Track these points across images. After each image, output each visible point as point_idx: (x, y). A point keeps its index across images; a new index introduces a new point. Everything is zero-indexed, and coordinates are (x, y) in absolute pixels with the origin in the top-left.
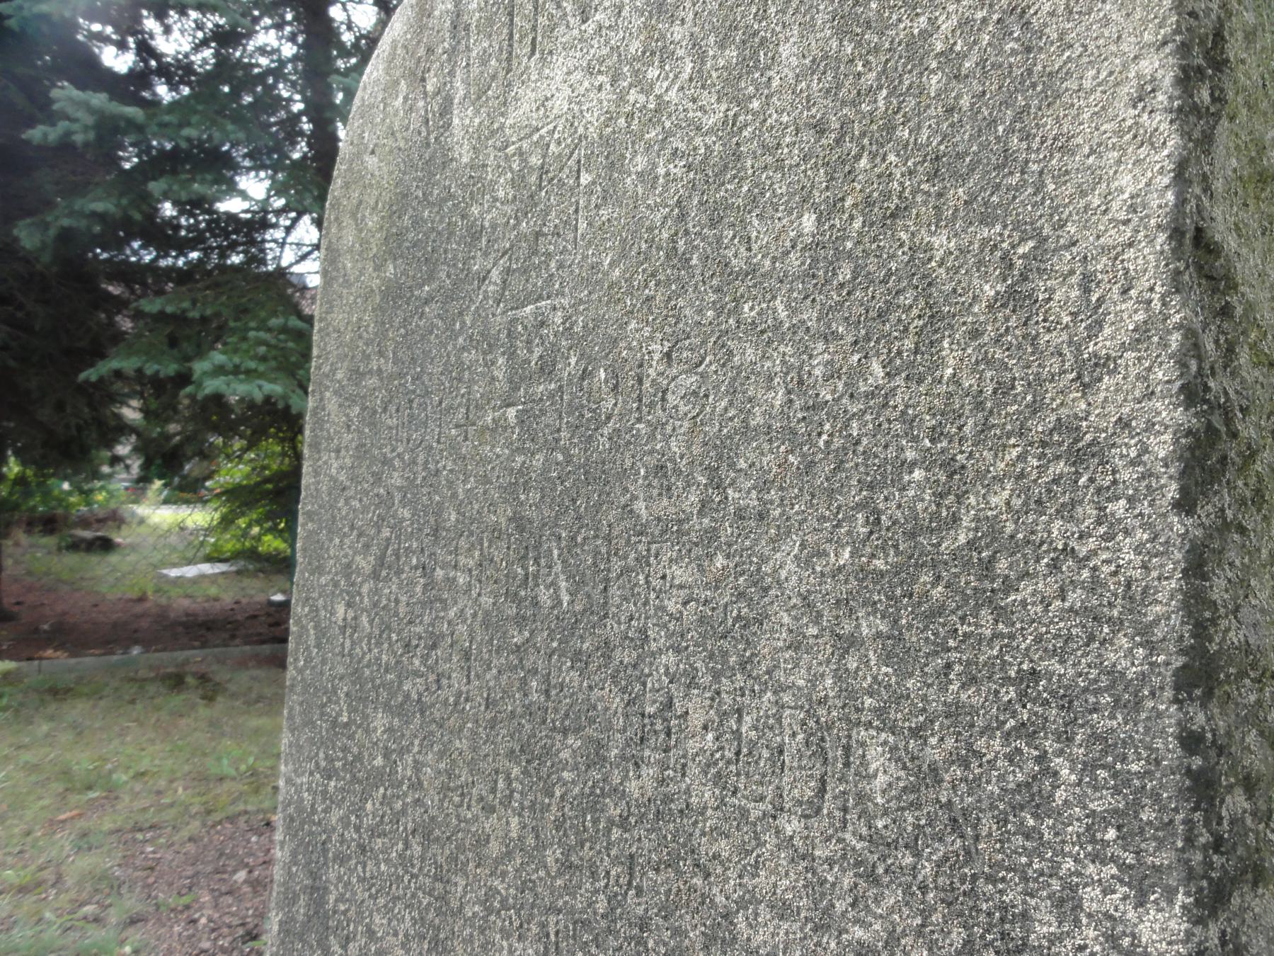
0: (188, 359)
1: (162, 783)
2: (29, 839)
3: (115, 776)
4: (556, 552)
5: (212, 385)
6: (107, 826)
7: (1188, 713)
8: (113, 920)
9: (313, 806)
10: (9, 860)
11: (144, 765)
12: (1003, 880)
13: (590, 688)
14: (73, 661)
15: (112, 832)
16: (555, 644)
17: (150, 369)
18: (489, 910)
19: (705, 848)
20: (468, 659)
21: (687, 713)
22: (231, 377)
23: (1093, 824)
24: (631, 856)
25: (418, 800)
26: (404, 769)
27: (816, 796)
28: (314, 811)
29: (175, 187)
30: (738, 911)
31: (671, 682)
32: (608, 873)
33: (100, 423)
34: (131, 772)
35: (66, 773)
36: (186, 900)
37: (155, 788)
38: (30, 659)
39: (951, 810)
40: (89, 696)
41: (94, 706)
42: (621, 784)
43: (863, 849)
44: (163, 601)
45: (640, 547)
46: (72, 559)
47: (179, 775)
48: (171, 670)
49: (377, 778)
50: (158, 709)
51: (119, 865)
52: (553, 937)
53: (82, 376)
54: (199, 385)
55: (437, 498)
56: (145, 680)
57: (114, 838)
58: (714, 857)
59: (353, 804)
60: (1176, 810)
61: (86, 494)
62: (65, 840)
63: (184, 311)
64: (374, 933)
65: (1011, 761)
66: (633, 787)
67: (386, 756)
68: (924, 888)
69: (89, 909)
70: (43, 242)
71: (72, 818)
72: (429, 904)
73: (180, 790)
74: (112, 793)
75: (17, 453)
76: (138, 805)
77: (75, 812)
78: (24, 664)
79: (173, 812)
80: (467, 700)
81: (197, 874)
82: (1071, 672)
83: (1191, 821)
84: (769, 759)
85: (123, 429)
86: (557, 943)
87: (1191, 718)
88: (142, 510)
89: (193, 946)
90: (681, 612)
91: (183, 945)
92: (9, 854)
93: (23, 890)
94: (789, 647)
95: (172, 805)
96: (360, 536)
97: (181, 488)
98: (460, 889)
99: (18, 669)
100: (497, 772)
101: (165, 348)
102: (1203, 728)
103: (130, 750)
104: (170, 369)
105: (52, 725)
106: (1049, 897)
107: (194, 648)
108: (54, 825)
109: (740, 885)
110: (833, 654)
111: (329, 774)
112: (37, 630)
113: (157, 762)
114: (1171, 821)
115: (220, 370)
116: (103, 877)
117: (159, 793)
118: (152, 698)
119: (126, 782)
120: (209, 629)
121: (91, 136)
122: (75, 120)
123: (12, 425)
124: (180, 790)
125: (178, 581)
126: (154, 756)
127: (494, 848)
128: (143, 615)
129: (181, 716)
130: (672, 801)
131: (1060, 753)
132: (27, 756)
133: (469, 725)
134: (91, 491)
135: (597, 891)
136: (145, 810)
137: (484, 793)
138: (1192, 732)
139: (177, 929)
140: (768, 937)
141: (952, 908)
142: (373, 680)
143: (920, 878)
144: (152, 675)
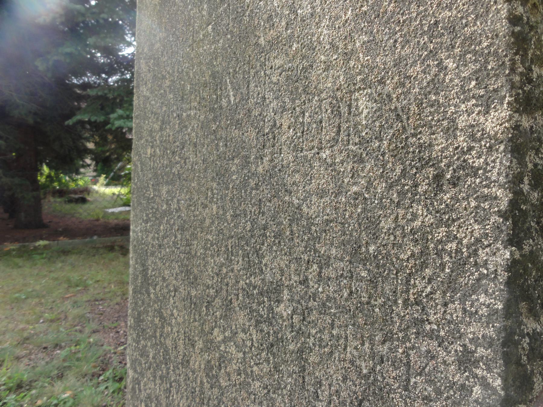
1: (106, 284)
2: (55, 304)
3: (87, 282)
4: (228, 81)
5: (118, 123)
6: (85, 299)
7: (514, 6)
8: (87, 331)
9: (142, 237)
10: (47, 311)
11: (99, 277)
12: (420, 133)
13: (243, 134)
14: (70, 241)
15: (86, 302)
16: (229, 122)
17: (93, 119)
18: (206, 249)
19: (289, 180)
20: (196, 147)
21: (282, 125)
22: (126, 120)
23: (464, 84)
24: (260, 200)
25: (179, 216)
26: (174, 205)
27: (336, 135)
28: (143, 239)
30: (303, 203)
31: (275, 114)
32: (251, 212)
34: (94, 281)
35: (69, 281)
36: (115, 325)
37: (103, 286)
38: (54, 240)
39: (396, 111)
40: (77, 254)
41: (79, 257)
42: (255, 170)
43: (356, 149)
45: (262, 59)
46: (72, 205)
47: (112, 281)
48: (109, 244)
49: (165, 213)
50: (104, 258)
51: (89, 313)
52: (230, 250)
53: (66, 123)
54: (113, 124)
55: (183, 82)
56: (99, 248)
57: (87, 304)
58: (293, 184)
59: (156, 229)
60: (506, 56)
62: (68, 304)
63: (106, 94)
64: (165, 278)
65: (425, 73)
66: (260, 169)
67: (167, 204)
68: (383, 155)
69: (78, 328)
71: (71, 296)
72: (184, 257)
73: (113, 286)
74: (86, 288)
75: (47, 165)
76: (96, 292)
78: (51, 242)
79: (110, 295)
80: (196, 165)
81: (119, 316)
82: (455, 12)
83: (514, 59)
84: (316, 128)
85: (87, 151)
86: (232, 251)
87: (516, 9)
88: (96, 187)
89: (118, 341)
90: (279, 80)
91: (114, 340)
92: (47, 309)
93: (52, 321)
94: (324, 71)
95: (110, 292)
96: (155, 115)
97: (113, 179)
98: (195, 246)
99: (49, 244)
100: (208, 190)
102: (522, 15)
103: (93, 272)
104: (101, 119)
105: (63, 264)
106: (442, 131)
107: (118, 236)
108: (64, 299)
109: (304, 191)
110: (343, 63)
111: (146, 222)
113: (103, 277)
114: (503, 63)
115: (121, 117)
116: (83, 316)
117: (105, 288)
118: (101, 254)
119: (91, 284)
120: (124, 230)
123: (42, 148)
124: (113, 286)
125: (113, 213)
126: (102, 275)
127: (208, 222)
129: (113, 261)
130: (276, 167)
131: (448, 57)
132: (52, 275)
133: (197, 175)
134: (77, 180)
135: (247, 222)
136: (99, 294)
137: (203, 201)
138: (516, 15)
139: (111, 335)
140: (316, 209)
141: (396, 158)
142: (161, 174)
143: (382, 150)
144: (101, 246)
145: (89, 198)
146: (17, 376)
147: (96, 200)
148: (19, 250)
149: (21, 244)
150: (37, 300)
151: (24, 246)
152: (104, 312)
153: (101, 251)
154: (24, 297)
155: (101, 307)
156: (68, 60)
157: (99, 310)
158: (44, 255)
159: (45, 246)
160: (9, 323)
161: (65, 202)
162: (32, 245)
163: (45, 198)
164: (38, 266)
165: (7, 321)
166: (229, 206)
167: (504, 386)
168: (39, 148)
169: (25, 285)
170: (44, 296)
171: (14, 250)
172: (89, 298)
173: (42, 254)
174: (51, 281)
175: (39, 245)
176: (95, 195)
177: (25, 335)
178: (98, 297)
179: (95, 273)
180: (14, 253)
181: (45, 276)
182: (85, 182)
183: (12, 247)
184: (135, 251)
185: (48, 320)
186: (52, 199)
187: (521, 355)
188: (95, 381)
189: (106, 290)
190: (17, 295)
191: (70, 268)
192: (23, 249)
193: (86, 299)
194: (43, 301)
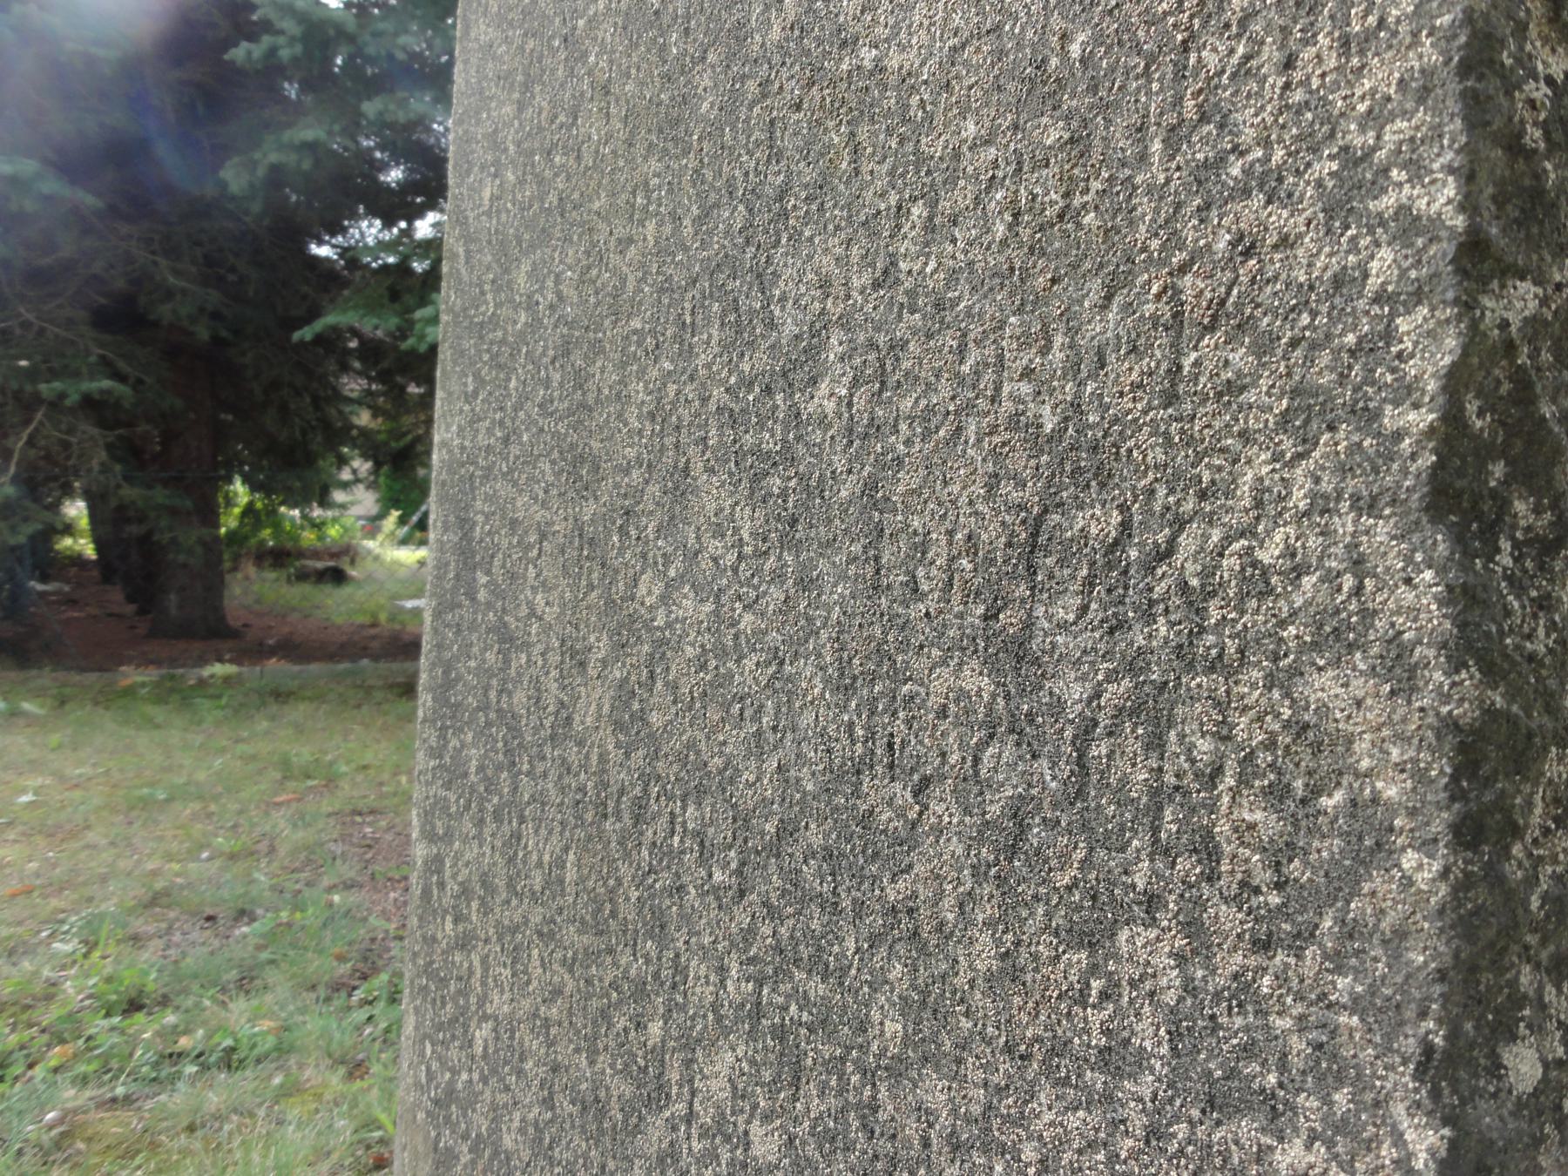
0: (411, 310)
11: (369, 757)
14: (296, 668)
15: (329, 815)
29: (392, 107)
33: (326, 425)
34: (353, 765)
35: (285, 764)
40: (310, 699)
41: (317, 709)
44: (397, 627)
46: (306, 588)
56: (371, 687)
57: (332, 821)
61: (318, 526)
62: (280, 821)
70: (252, 185)
71: (289, 801)
75: (246, 480)
77: (291, 796)
93: (233, 857)
95: (395, 794)
99: (239, 674)
101: (386, 301)
112: (261, 644)
121: (298, 49)
122: (281, 32)
123: (230, 417)
128: (374, 637)
132: (241, 748)
139: (392, 895)
145: (353, 573)
146: (129, 978)
147: (370, 578)
148: (157, 685)
149: (164, 671)
150: (197, 806)
151: (172, 677)
152: (377, 840)
153: (378, 695)
154: (162, 797)
155: (368, 830)
156: (307, 165)
157: (364, 837)
158: (224, 701)
159: (227, 680)
160: (118, 856)
161: (289, 581)
162: (192, 675)
163: (235, 569)
164: (204, 726)
165: (113, 851)
166: (690, 199)
167: (1467, 196)
168: (223, 416)
169: (167, 770)
170: (216, 798)
171: (143, 685)
172: (337, 807)
173: (219, 697)
174: (239, 763)
175: (212, 676)
176: (369, 565)
177: (159, 885)
178: (361, 805)
180: (144, 691)
181: (223, 750)
182: (346, 530)
183: (139, 679)
184: (442, 500)
185: (222, 854)
186: (251, 570)
187: (1522, 122)
188: (339, 1001)
189: (384, 789)
190: (145, 791)
191: (290, 731)
192: (169, 684)
193: (330, 809)
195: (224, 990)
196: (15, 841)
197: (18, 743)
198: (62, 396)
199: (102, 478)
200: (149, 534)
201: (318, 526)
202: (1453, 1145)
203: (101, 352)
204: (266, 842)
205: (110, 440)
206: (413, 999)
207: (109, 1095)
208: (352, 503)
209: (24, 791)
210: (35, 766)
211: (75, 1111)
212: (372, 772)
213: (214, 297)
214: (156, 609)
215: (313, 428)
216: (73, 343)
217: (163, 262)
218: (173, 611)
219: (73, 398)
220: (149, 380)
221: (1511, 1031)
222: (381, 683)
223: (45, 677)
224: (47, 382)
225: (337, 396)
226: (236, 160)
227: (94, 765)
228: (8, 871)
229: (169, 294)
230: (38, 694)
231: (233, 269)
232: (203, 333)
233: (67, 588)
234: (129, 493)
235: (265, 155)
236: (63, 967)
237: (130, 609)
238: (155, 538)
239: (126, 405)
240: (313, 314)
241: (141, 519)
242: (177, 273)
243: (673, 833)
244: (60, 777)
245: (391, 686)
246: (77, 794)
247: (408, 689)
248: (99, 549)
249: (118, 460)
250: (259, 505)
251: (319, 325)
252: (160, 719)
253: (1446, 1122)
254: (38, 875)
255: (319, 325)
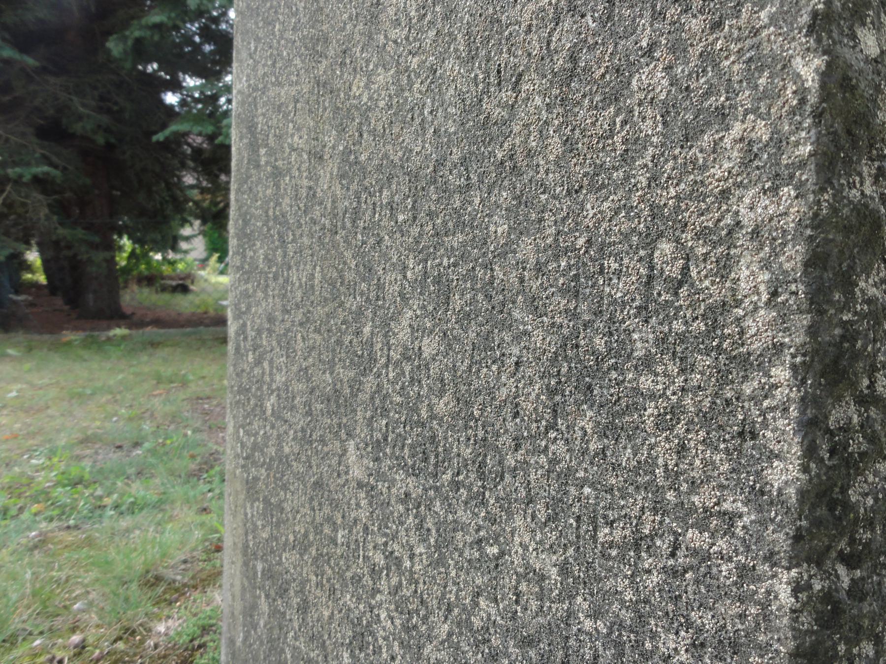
11: (205, 372)
33: (174, 199)
40: (171, 346)
46: (166, 296)
53: (155, 138)
62: (156, 402)
99: (130, 335)
123: (119, 193)
132: (132, 370)
147: (203, 290)
149: (87, 333)
150: (110, 397)
151: (92, 336)
152: (212, 411)
158: (122, 347)
159: (124, 338)
162: (103, 336)
163: (126, 287)
171: (76, 340)
172: (188, 395)
173: (119, 345)
175: (115, 336)
177: (89, 432)
178: (201, 395)
179: (198, 370)
180: (77, 343)
186: (135, 287)
190: (80, 390)
193: (184, 397)
194: (118, 397)
195: (128, 478)
196: (7, 415)
197: (6, 368)
198: (21, 176)
199: (46, 223)
200: (75, 255)
201: (172, 263)
202: (829, 65)
203: (42, 152)
204: (149, 413)
205: (49, 201)
206: (232, 411)
207: (66, 525)
208: (191, 250)
209: (11, 391)
210: (15, 380)
211: (47, 533)
212: (207, 379)
213: (105, 119)
214: (83, 301)
215: (167, 202)
216: (25, 146)
217: (75, 98)
218: (91, 304)
219: (27, 178)
220: (70, 168)
221: (862, 20)
222: (211, 337)
223: (20, 337)
224: (13, 168)
225: (180, 185)
226: (115, 36)
227: (50, 379)
228: (3, 428)
229: (80, 118)
230: (15, 346)
231: (116, 103)
232: (100, 140)
233: (30, 298)
234: (62, 231)
235: (132, 33)
236: (37, 471)
237: (67, 308)
238: (79, 258)
239: (58, 181)
240: (164, 126)
241: (69, 247)
242: (84, 105)
243: (375, 214)
244: (32, 385)
245: (217, 339)
246: (41, 392)
247: (224, 341)
248: (48, 278)
249: (54, 213)
250: (138, 251)
251: (167, 132)
252: (86, 357)
253: (825, 53)
254: (21, 430)
255: (167, 132)
